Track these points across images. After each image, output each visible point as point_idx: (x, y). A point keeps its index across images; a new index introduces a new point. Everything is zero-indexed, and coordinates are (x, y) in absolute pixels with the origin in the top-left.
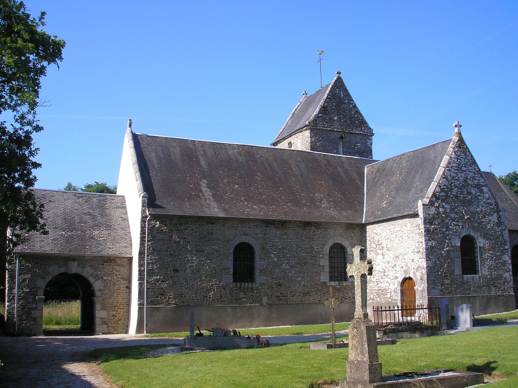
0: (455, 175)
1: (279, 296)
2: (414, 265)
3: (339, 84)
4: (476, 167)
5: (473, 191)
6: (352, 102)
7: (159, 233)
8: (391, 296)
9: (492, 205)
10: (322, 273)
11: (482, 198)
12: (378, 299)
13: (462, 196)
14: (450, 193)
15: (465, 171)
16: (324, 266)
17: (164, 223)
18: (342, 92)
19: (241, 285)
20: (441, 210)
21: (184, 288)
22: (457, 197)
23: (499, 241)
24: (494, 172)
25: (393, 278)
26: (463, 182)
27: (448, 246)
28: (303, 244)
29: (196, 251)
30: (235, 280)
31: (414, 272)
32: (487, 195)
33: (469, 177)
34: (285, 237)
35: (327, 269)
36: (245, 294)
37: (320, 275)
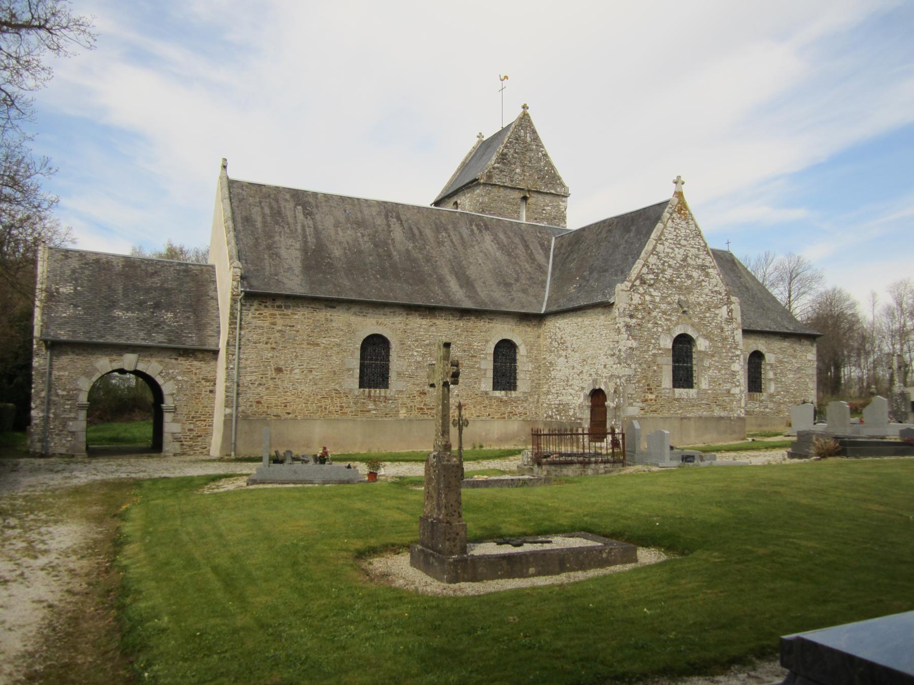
0: (670, 251)
1: (421, 409)
2: (605, 373)
3: (524, 121)
4: (701, 241)
5: (695, 274)
6: (542, 149)
7: (255, 318)
8: (575, 414)
9: (720, 294)
10: (483, 380)
11: (707, 283)
12: (558, 417)
13: (679, 280)
14: (661, 275)
15: (685, 246)
16: (486, 370)
17: (263, 304)
18: (528, 135)
19: (370, 392)
20: (648, 298)
21: (290, 394)
22: (671, 281)
23: (727, 344)
24: (732, 251)
25: (577, 388)
26: (682, 261)
27: (654, 348)
28: (458, 340)
29: (308, 344)
30: (362, 385)
31: (606, 382)
32: (714, 281)
33: (690, 255)
34: (433, 329)
35: (490, 374)
36: (375, 405)
37: (480, 381)
